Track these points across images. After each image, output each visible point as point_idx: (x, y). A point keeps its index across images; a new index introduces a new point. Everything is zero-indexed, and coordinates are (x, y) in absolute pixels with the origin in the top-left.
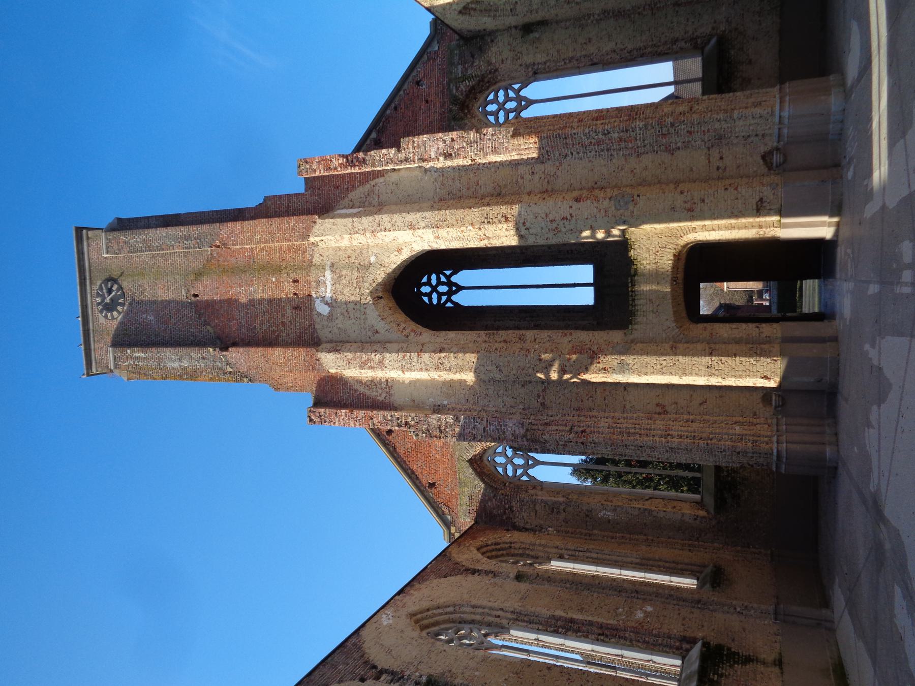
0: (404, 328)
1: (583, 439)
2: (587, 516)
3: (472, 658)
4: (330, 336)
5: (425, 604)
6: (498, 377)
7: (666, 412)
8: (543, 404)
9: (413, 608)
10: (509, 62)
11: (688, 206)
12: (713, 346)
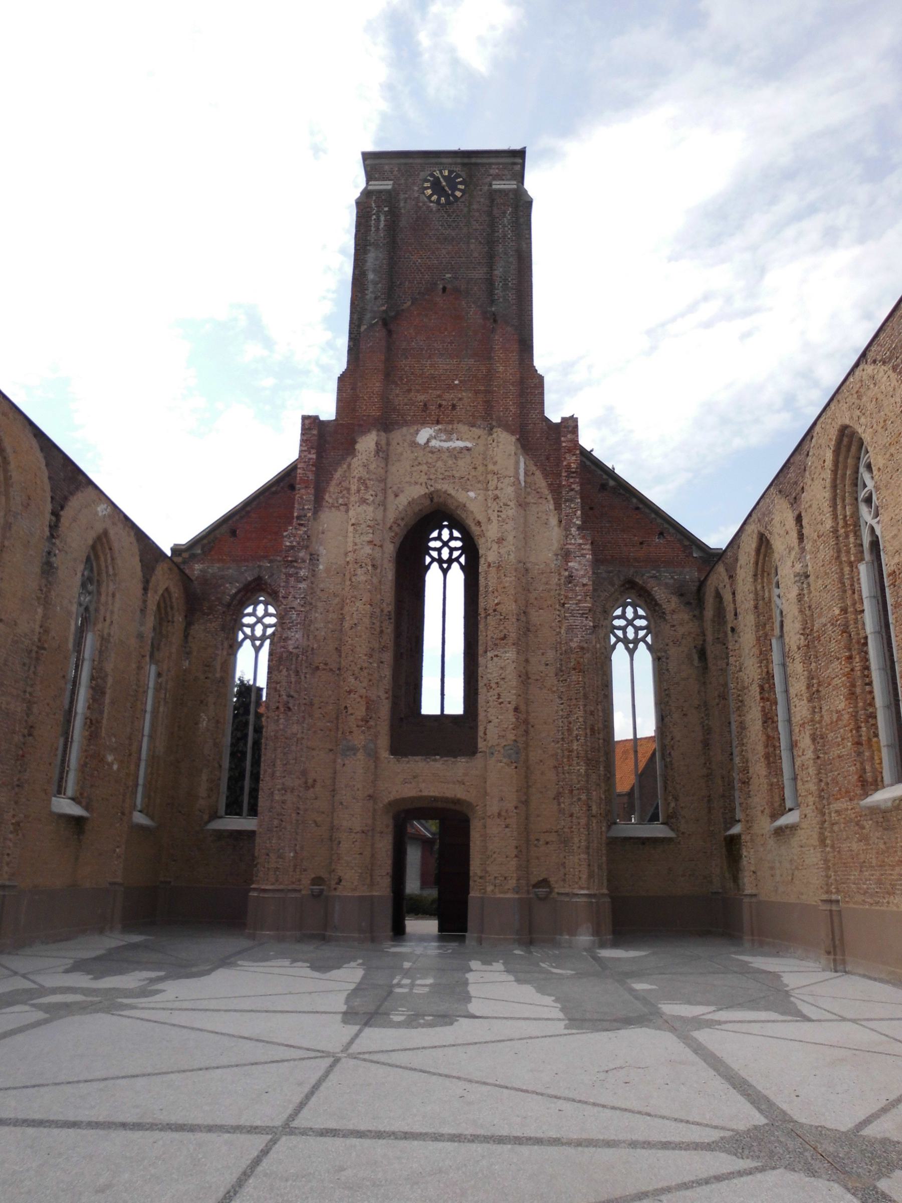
0: (399, 525)
1: (282, 709)
2: (202, 702)
3: (70, 602)
4: (394, 443)
5: (116, 546)
6: (346, 625)
7: (307, 788)
8: (317, 668)
9: (112, 533)
10: (672, 633)
11: (503, 813)
12: (370, 834)
